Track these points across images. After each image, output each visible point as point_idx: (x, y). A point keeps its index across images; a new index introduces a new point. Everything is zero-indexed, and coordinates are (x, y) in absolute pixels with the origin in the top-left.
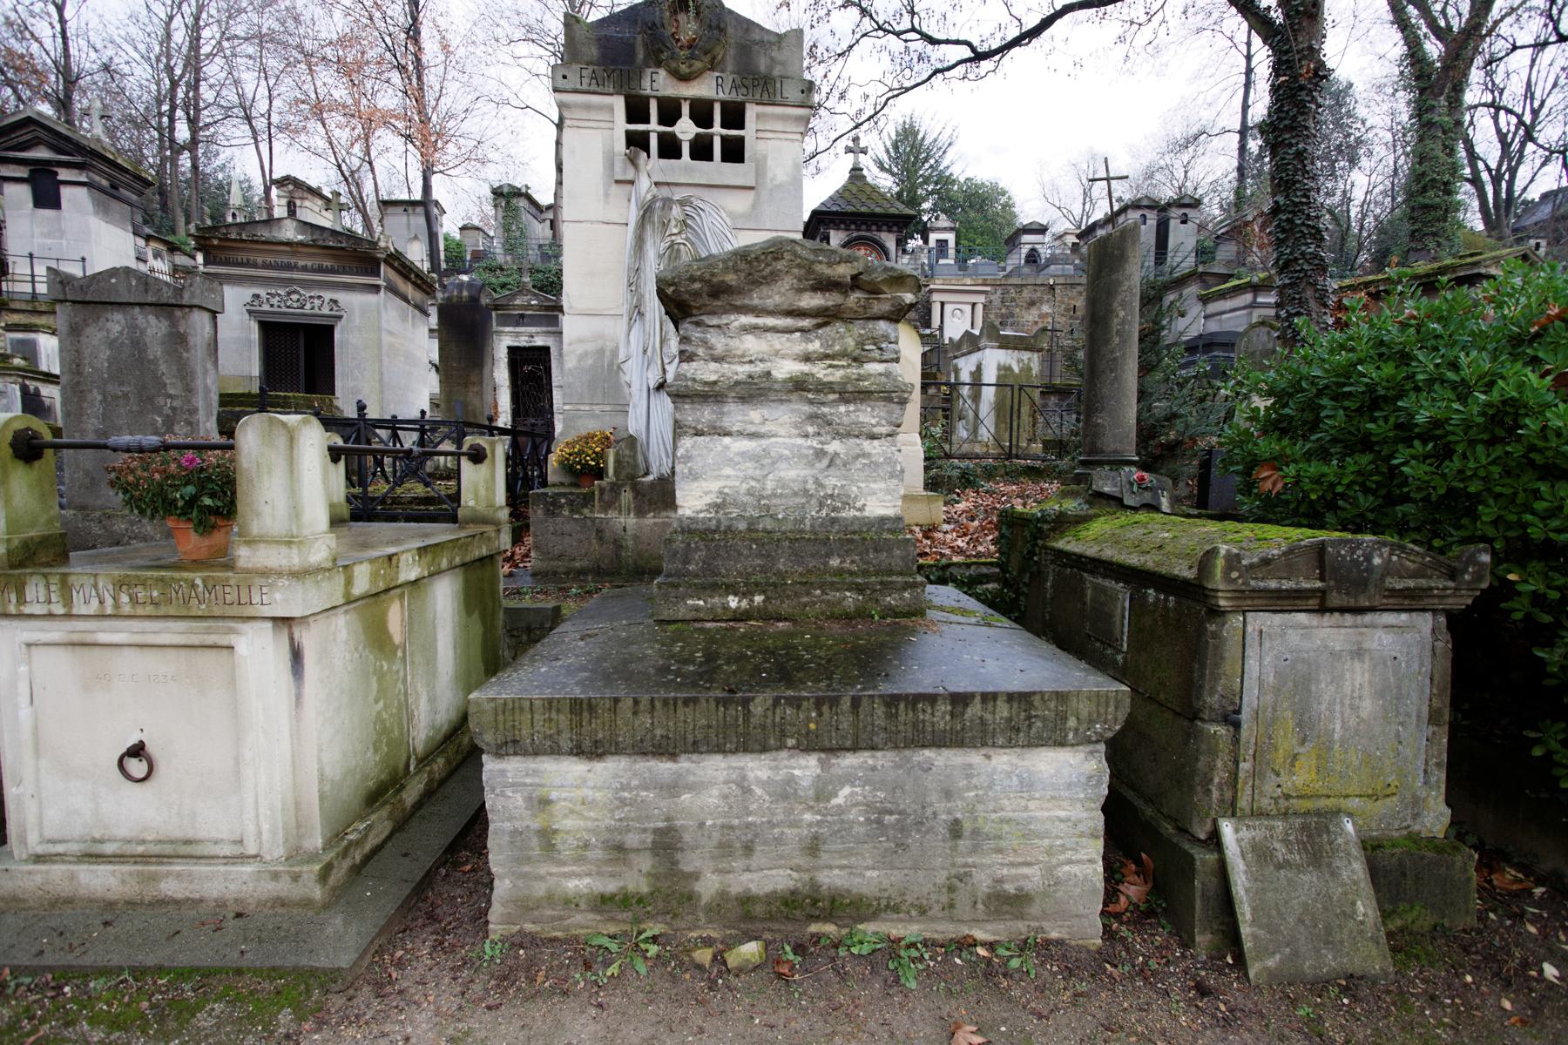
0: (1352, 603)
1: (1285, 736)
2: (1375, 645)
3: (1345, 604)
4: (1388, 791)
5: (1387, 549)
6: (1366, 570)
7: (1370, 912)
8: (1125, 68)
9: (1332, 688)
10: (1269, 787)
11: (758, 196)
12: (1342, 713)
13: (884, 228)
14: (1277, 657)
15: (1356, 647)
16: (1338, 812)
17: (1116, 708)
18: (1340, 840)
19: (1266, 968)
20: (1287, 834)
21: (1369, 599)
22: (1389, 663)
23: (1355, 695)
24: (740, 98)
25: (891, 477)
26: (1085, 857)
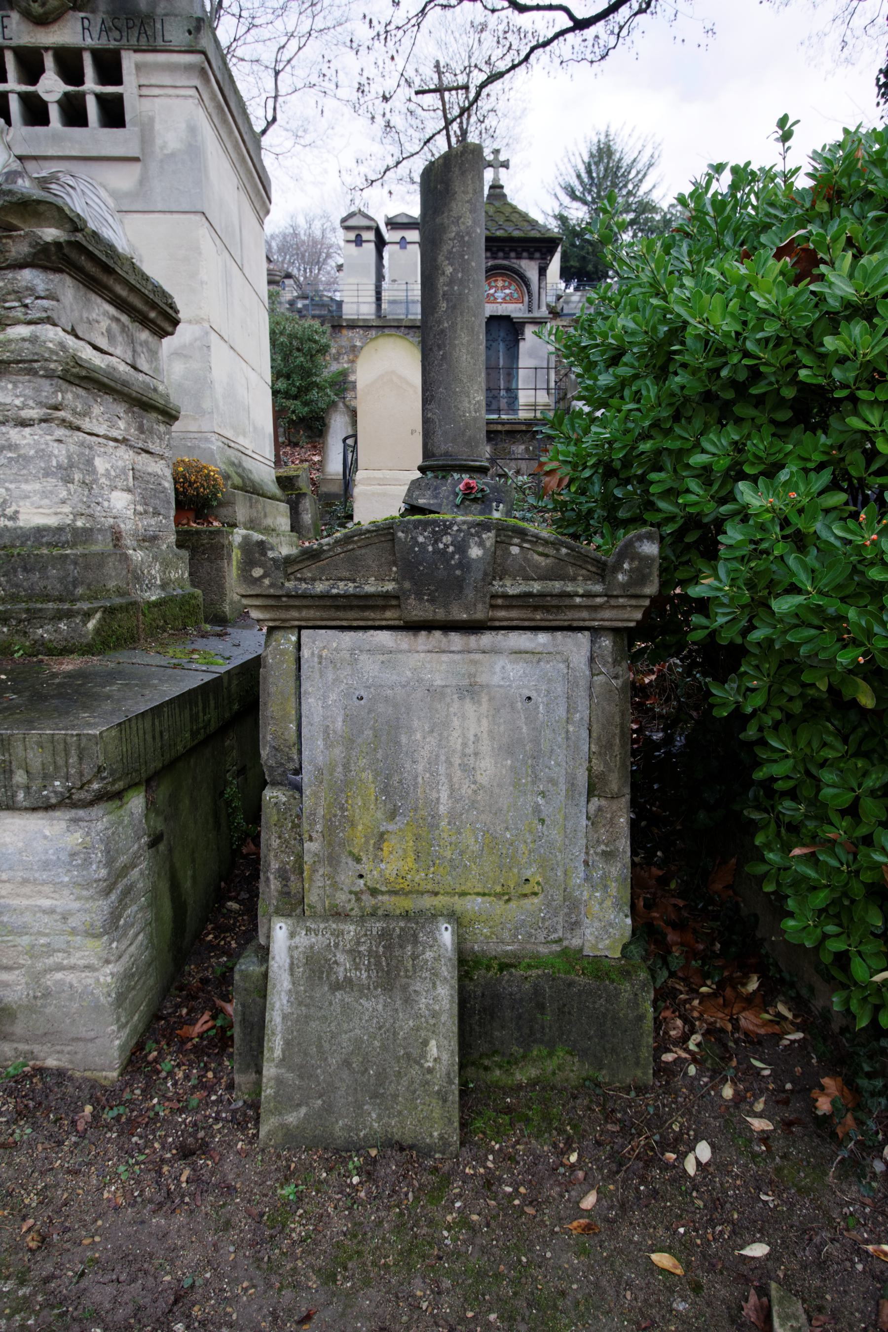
0: (440, 615)
1: (365, 807)
2: (496, 680)
3: (429, 616)
4: (527, 889)
5: (492, 534)
6: (461, 565)
7: (445, 1057)
8: (843, 56)
9: (432, 740)
10: (346, 877)
11: (145, 170)
12: (449, 777)
13: (525, 254)
14: (347, 695)
15: (466, 682)
16: (433, 916)
17: (81, 759)
18: (429, 955)
19: (283, 1126)
20: (358, 943)
21: (467, 609)
22: (519, 705)
23: (467, 751)
24: (113, 44)
25: (47, 474)
26: (82, 962)
